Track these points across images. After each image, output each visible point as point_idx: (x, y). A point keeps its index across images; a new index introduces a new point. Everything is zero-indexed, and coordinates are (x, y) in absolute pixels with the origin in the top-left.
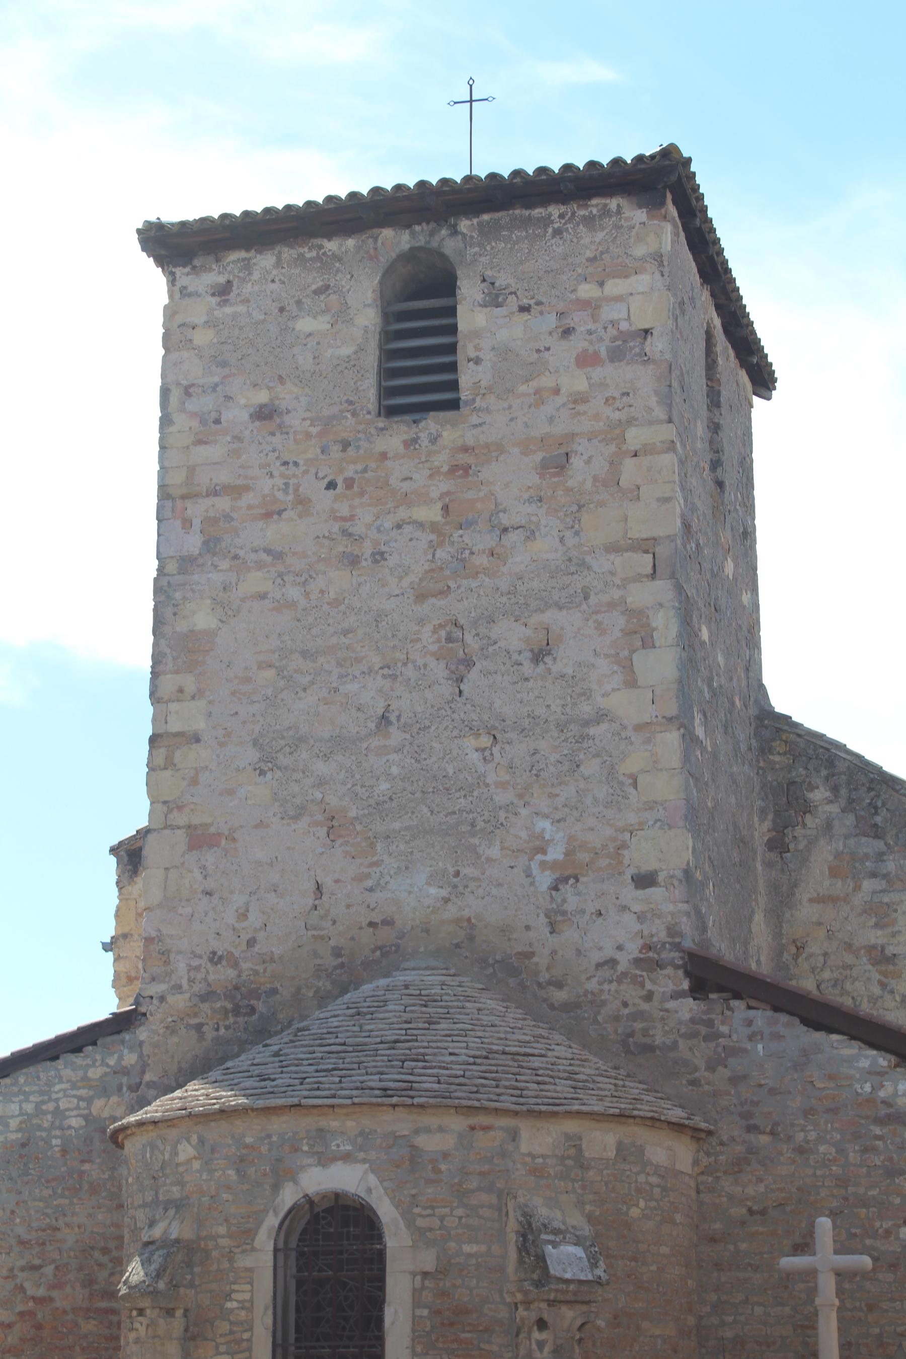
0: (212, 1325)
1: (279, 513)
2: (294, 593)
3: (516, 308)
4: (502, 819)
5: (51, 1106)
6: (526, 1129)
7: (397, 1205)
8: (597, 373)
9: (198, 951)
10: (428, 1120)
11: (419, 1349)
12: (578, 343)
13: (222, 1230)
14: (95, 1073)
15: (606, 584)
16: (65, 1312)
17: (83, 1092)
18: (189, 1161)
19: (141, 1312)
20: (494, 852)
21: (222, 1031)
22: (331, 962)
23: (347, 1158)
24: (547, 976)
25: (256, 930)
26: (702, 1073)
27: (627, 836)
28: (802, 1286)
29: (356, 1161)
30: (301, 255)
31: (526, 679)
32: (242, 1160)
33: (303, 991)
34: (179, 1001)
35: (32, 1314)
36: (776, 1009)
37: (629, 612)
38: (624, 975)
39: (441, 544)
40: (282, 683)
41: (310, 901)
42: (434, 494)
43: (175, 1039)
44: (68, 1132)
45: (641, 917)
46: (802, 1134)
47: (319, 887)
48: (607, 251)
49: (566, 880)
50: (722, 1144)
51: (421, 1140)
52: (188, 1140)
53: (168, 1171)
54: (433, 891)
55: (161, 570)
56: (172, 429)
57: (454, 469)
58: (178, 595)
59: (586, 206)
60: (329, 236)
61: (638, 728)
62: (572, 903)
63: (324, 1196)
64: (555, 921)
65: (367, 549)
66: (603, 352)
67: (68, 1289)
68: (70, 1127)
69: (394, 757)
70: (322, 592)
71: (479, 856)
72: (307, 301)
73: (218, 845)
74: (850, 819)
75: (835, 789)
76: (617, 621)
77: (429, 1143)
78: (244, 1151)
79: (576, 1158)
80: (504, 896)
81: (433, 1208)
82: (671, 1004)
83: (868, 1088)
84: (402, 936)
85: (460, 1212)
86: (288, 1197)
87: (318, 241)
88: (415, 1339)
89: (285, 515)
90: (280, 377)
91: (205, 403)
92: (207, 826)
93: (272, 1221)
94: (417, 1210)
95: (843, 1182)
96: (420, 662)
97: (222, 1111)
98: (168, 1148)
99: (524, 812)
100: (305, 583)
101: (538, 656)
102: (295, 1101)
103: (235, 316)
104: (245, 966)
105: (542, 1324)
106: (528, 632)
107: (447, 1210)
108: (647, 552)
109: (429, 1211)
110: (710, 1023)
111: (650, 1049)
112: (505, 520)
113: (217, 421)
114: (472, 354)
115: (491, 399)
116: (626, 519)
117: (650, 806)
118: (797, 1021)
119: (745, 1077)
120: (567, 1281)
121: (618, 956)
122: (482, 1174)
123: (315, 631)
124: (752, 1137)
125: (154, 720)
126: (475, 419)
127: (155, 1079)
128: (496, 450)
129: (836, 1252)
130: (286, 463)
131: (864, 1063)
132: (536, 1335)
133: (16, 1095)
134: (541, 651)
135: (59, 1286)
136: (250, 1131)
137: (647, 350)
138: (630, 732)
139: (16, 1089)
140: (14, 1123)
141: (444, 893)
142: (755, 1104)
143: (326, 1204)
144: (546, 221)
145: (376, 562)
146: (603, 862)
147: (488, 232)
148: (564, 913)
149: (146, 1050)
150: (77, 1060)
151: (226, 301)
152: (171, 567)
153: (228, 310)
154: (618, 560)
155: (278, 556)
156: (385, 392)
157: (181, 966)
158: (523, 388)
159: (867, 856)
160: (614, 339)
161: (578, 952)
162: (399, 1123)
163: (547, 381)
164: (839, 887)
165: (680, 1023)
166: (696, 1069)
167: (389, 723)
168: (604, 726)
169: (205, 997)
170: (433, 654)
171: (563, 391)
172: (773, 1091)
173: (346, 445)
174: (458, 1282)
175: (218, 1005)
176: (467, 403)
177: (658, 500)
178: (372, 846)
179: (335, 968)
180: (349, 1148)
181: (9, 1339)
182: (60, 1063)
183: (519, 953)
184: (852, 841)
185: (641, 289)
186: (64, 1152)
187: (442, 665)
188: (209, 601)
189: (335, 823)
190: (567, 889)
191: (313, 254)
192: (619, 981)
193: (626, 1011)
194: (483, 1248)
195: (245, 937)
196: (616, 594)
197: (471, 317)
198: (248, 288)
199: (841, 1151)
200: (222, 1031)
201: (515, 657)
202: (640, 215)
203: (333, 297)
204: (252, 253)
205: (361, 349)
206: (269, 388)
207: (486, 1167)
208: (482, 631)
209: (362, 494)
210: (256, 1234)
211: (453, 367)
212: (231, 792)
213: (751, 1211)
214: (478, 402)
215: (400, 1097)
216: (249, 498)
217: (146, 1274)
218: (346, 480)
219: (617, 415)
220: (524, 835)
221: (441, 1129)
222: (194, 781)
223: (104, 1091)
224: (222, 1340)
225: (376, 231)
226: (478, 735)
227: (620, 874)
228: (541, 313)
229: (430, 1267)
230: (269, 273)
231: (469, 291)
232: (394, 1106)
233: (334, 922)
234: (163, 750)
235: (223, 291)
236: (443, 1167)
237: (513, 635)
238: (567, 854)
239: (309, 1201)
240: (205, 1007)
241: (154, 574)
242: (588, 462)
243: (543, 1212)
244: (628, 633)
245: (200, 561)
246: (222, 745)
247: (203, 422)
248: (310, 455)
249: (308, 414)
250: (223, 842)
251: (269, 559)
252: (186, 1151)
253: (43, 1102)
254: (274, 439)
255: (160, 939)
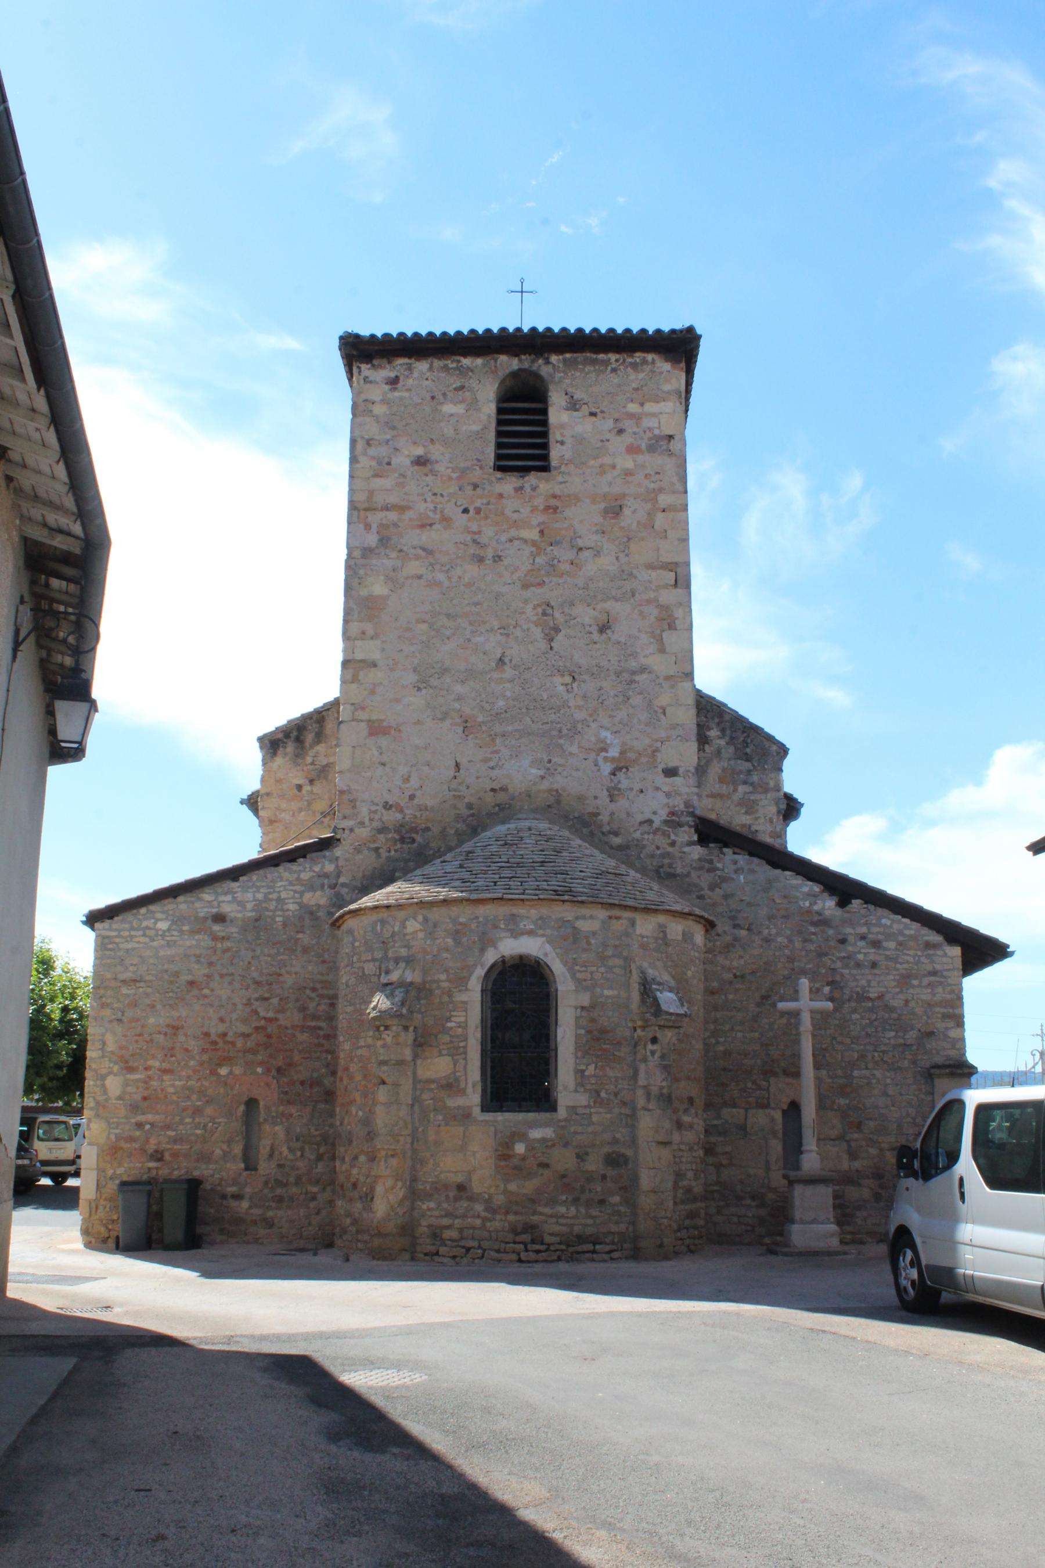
0: (436, 1037)
1: (431, 525)
2: (441, 577)
3: (587, 413)
4: (579, 729)
5: (275, 896)
6: (639, 918)
7: (565, 963)
8: (640, 458)
9: (376, 801)
10: (584, 911)
11: (579, 1054)
12: (627, 439)
13: (443, 977)
14: (305, 876)
15: (646, 588)
16: (287, 1028)
17: (298, 888)
18: (415, 932)
19: (387, 1028)
20: (574, 749)
21: (393, 853)
22: (466, 812)
23: (531, 933)
24: (608, 828)
25: (415, 790)
26: (706, 892)
27: (659, 744)
28: (766, 1020)
29: (537, 935)
30: (446, 366)
31: (595, 643)
32: (457, 932)
33: (448, 830)
34: (364, 832)
35: (264, 1028)
36: (751, 854)
37: (661, 607)
38: (658, 829)
39: (538, 554)
40: (433, 633)
41: (452, 773)
42: (535, 522)
43: (361, 857)
44: (287, 913)
45: (668, 795)
46: (767, 931)
47: (457, 766)
48: (646, 385)
49: (620, 769)
50: (718, 935)
51: (579, 924)
52: (415, 919)
53: (396, 938)
54: (534, 771)
55: (350, 556)
56: (358, 466)
57: (547, 508)
58: (362, 572)
59: (633, 357)
60: (465, 356)
61: (667, 678)
62: (624, 784)
63: (512, 957)
64: (614, 793)
65: (490, 553)
66: (644, 447)
67: (288, 1013)
68: (288, 910)
69: (508, 685)
70: (460, 577)
71: (564, 752)
72: (450, 395)
73: (389, 733)
74: (731, 749)
75: (723, 731)
76: (653, 612)
77: (584, 926)
78: (459, 927)
79: (663, 937)
80: (580, 778)
81: (586, 967)
82: (687, 849)
83: (807, 904)
84: (513, 798)
85: (602, 969)
86: (491, 957)
87: (458, 358)
88: (577, 1048)
89: (434, 527)
90: (432, 440)
91: (382, 451)
92: (382, 721)
93: (480, 972)
94: (577, 968)
95: (791, 960)
96: (525, 627)
97: (445, 901)
98: (398, 924)
99: (594, 725)
100: (447, 571)
101: (603, 629)
102: (500, 895)
103: (401, 399)
104: (408, 812)
105: (654, 1040)
106: (596, 614)
107: (595, 968)
108: (671, 571)
109: (584, 969)
110: (711, 862)
111: (673, 876)
112: (580, 543)
113: (389, 464)
114: (559, 438)
115: (571, 468)
116: (658, 550)
117: (674, 727)
118: (764, 862)
119: (732, 895)
120: (671, 1014)
121: (654, 818)
122: (615, 946)
123: (454, 602)
124: (736, 931)
125: (345, 651)
126: (560, 479)
127: (347, 881)
128: (574, 499)
129: (811, 1000)
130: (435, 494)
131: (805, 889)
132: (650, 1047)
133: (251, 887)
134: (604, 626)
135: (282, 1011)
136: (463, 915)
137: (671, 448)
138: (661, 681)
139: (250, 884)
140: (249, 906)
141: (541, 773)
142: (739, 911)
143: (512, 963)
144: (607, 363)
145: (495, 561)
146: (644, 760)
147: (569, 364)
148: (619, 790)
149: (341, 863)
150: (294, 867)
151: (395, 389)
152: (357, 554)
153: (397, 394)
154: (653, 574)
155: (429, 552)
156: (499, 457)
157: (364, 810)
158: (592, 463)
159: (741, 772)
160: (650, 439)
161: (628, 814)
162: (565, 912)
163: (607, 460)
164: (724, 789)
165: (693, 860)
166: (702, 889)
167: (504, 663)
168: (645, 676)
169: (382, 830)
170: (534, 623)
171: (618, 467)
172: (749, 904)
173: (475, 486)
174: (602, 1013)
175: (390, 836)
176: (556, 468)
177: (679, 540)
178: (493, 740)
179: (468, 816)
180: (532, 927)
181: (249, 1043)
182: (281, 869)
183: (590, 813)
184: (732, 762)
185: (667, 411)
186: (285, 925)
187: (539, 630)
188: (382, 578)
189: (468, 724)
190: (621, 775)
191: (454, 365)
192: (654, 833)
193: (658, 852)
194: (615, 992)
195: (408, 793)
196: (652, 595)
197: (557, 415)
198: (410, 382)
199: (790, 941)
200: (393, 853)
201: (588, 628)
202: (666, 366)
203: (468, 394)
204: (412, 361)
205: (485, 428)
206: (424, 446)
207: (617, 943)
208: (566, 610)
209: (486, 518)
210: (469, 980)
211: (545, 446)
212: (397, 701)
213: (735, 976)
214: (563, 468)
215: (564, 895)
216: (409, 515)
217: (393, 1004)
218: (475, 508)
219: (652, 486)
220: (593, 739)
221: (591, 917)
222: (373, 692)
223: (311, 887)
224: (445, 1047)
225: (496, 356)
226: (563, 676)
227: (655, 767)
228: (604, 418)
229: (586, 1004)
230: (424, 374)
231: (556, 401)
232: (564, 901)
233: (468, 787)
234: (351, 671)
235: (394, 382)
236: (593, 941)
237: (586, 615)
238: (621, 753)
239: (503, 960)
240: (381, 837)
241: (345, 557)
242: (634, 512)
243: (651, 972)
244: (660, 619)
245: (377, 551)
246: (392, 670)
247: (379, 463)
248: (451, 491)
249: (450, 465)
250: (393, 732)
251: (423, 554)
252: (412, 926)
253: (270, 893)
254: (427, 479)
255: (349, 791)
